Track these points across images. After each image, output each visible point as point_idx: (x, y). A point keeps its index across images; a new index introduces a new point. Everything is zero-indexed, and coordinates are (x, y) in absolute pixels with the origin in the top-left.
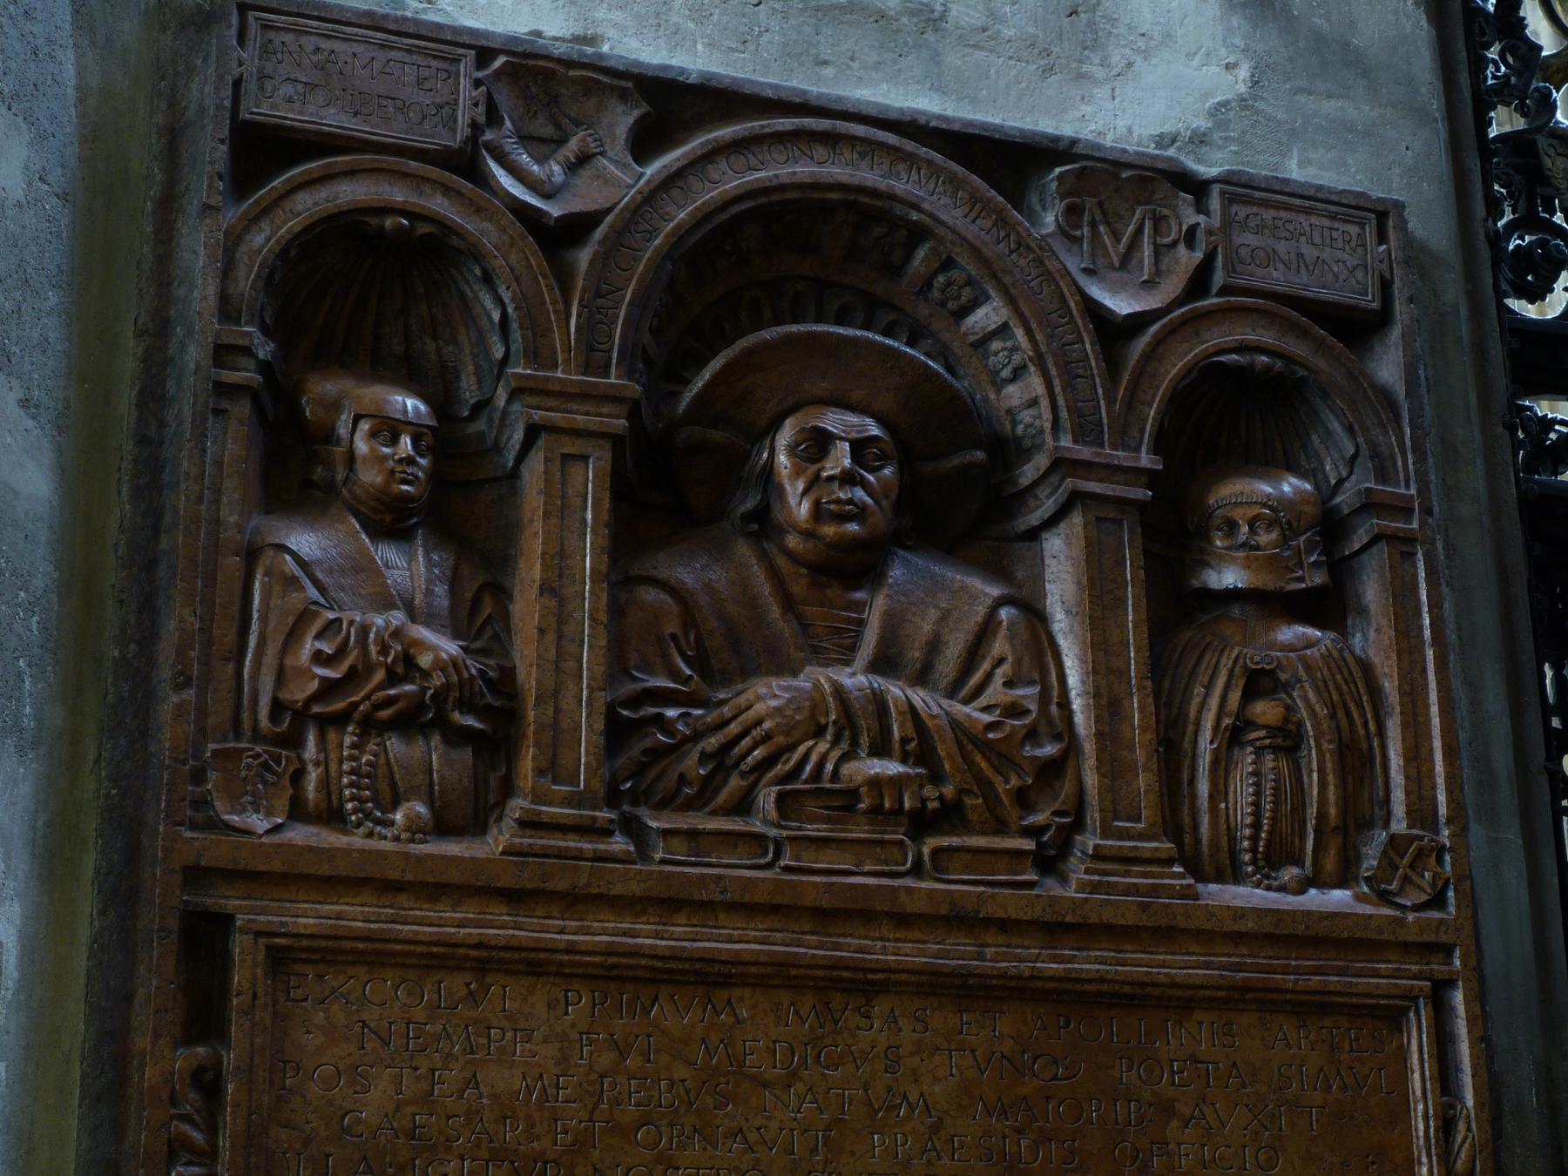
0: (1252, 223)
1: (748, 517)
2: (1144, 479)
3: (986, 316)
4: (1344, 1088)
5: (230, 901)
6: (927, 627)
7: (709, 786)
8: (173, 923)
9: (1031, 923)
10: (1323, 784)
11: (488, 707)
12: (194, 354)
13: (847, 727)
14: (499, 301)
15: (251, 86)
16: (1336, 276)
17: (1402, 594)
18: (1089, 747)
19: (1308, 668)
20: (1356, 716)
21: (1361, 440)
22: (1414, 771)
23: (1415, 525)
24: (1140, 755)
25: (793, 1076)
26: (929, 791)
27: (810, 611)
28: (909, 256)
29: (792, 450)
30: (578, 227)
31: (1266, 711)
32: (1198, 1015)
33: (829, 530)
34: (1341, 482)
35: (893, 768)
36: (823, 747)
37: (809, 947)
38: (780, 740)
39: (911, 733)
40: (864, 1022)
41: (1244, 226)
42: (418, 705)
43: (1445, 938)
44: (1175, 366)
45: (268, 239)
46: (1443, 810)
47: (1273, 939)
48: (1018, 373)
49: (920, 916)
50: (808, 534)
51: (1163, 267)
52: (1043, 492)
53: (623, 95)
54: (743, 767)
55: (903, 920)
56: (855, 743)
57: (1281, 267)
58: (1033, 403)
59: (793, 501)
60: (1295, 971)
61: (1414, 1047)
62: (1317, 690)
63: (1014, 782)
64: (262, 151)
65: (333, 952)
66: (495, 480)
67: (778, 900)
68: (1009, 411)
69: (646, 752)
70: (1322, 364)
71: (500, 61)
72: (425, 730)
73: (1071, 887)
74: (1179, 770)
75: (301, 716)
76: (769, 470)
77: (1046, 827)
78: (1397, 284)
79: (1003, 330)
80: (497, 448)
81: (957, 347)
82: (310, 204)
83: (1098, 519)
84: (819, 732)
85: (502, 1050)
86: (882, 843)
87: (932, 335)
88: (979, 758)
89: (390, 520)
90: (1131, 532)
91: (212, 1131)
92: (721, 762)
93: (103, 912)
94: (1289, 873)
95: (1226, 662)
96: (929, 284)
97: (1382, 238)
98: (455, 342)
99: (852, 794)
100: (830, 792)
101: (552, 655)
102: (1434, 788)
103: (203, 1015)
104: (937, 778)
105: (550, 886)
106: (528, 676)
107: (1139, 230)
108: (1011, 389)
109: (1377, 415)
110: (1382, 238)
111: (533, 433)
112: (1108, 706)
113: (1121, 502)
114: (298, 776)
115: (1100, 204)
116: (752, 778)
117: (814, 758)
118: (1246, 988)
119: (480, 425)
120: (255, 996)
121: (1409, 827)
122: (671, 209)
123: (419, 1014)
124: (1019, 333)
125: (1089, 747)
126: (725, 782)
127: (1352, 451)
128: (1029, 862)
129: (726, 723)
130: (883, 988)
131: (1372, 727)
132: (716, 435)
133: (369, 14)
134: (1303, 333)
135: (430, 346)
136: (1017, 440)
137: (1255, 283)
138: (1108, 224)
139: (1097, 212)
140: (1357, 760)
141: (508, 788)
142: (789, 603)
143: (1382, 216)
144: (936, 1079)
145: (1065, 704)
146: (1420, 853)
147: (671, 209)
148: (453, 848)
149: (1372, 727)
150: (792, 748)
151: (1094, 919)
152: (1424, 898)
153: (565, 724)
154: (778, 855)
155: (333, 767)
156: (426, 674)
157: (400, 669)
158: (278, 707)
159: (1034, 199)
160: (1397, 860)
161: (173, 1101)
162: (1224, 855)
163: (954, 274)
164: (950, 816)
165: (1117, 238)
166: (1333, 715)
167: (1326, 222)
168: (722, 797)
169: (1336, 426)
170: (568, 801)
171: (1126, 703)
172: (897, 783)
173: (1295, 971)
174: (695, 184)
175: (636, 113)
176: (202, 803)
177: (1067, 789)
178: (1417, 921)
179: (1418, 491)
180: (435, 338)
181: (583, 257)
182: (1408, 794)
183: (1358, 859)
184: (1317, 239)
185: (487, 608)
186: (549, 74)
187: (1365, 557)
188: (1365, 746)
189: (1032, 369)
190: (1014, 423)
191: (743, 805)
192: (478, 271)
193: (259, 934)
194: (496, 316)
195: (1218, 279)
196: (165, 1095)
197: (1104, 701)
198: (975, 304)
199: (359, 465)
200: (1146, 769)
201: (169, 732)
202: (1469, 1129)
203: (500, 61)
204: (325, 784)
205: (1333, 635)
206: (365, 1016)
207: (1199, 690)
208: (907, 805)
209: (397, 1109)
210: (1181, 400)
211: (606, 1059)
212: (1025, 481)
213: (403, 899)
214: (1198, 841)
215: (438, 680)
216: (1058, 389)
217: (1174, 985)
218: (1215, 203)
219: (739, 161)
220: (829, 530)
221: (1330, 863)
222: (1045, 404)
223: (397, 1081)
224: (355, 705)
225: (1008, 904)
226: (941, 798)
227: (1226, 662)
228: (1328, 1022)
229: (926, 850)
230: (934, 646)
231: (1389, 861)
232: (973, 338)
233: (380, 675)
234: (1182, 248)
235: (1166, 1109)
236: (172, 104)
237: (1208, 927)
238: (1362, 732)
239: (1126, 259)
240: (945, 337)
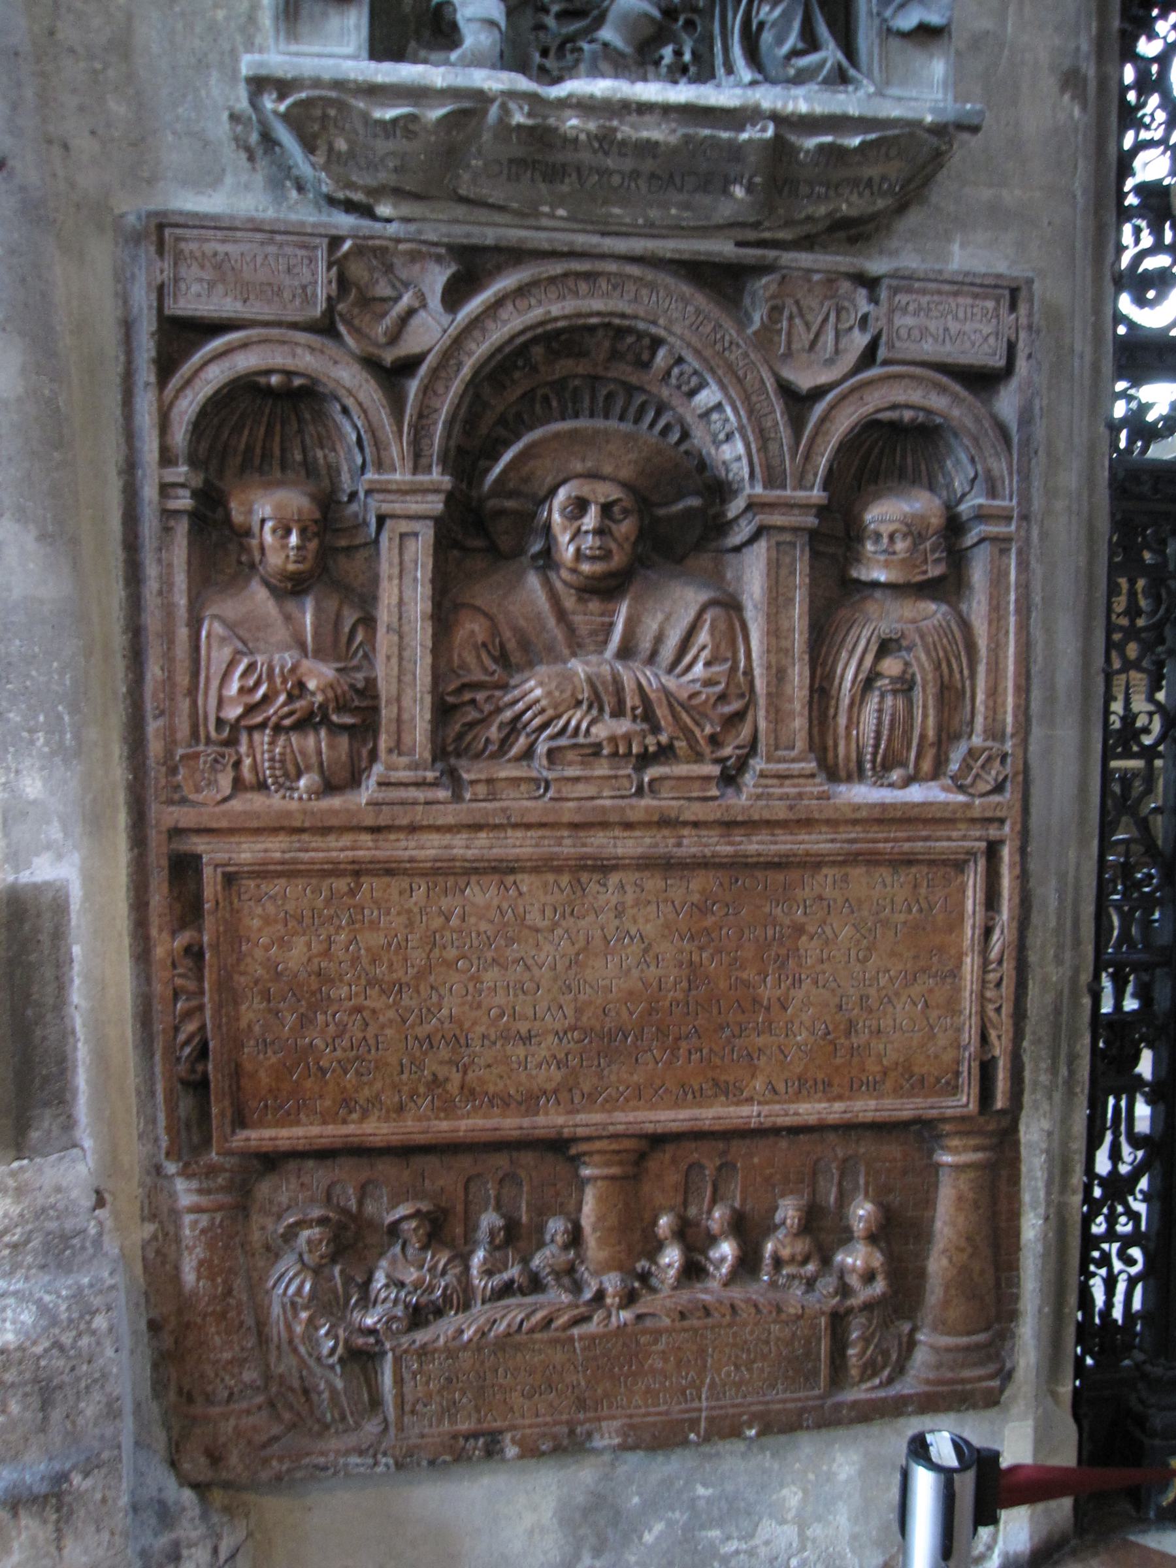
0: (911, 308)
1: (535, 557)
2: (814, 511)
3: (708, 396)
4: (921, 910)
5: (199, 845)
6: (655, 626)
7: (505, 743)
8: (165, 863)
9: (714, 822)
10: (925, 716)
11: (357, 708)
12: (149, 492)
13: (596, 701)
14: (355, 427)
15: (169, 289)
16: (973, 345)
17: (998, 579)
18: (762, 701)
19: (922, 637)
20: (955, 666)
21: (979, 467)
22: (993, 697)
23: (1013, 527)
24: (797, 706)
25: (555, 925)
26: (650, 740)
27: (578, 619)
28: (653, 354)
29: (562, 512)
30: (408, 366)
31: (891, 666)
32: (825, 871)
33: (586, 567)
34: (964, 495)
35: (624, 726)
36: (579, 714)
37: (568, 847)
38: (550, 712)
39: (637, 702)
40: (602, 890)
41: (904, 311)
42: (311, 714)
43: (999, 814)
44: (844, 423)
45: (191, 403)
46: (1009, 729)
47: (880, 821)
48: (729, 437)
49: (639, 823)
50: (574, 571)
51: (841, 346)
52: (743, 522)
53: (439, 259)
54: (528, 729)
55: (628, 826)
56: (601, 710)
57: (930, 340)
58: (739, 459)
59: (563, 548)
60: (895, 840)
61: (971, 883)
62: (928, 653)
63: (708, 730)
64: (181, 335)
65: (262, 872)
66: (365, 545)
67: (544, 820)
68: (724, 463)
69: (464, 725)
70: (956, 412)
71: (347, 245)
72: (316, 728)
73: (743, 800)
74: (827, 708)
75: (235, 726)
76: (548, 527)
77: (729, 758)
78: (1021, 345)
79: (719, 407)
80: (366, 524)
81: (689, 419)
82: (215, 376)
83: (778, 544)
84: (579, 703)
85: (371, 922)
86: (616, 777)
87: (673, 409)
88: (684, 715)
89: (291, 587)
90: (802, 551)
91: (200, 979)
92: (514, 727)
93: (131, 849)
94: (896, 775)
95: (866, 633)
96: (668, 373)
97: (1013, 307)
98: (334, 450)
99: (599, 746)
100: (582, 746)
101: (395, 672)
102: (1005, 712)
103: (189, 910)
104: (656, 729)
105: (397, 823)
106: (386, 688)
107: (828, 315)
108: (725, 447)
109: (994, 446)
110: (1013, 307)
111: (381, 520)
112: (779, 675)
113: (795, 530)
114: (237, 764)
115: (797, 302)
116: (533, 737)
117: (573, 723)
118: (858, 854)
119: (354, 507)
120: (217, 903)
121: (985, 740)
122: (473, 346)
123: (320, 902)
124: (728, 410)
125: (762, 701)
126: (517, 739)
127: (972, 475)
128: (714, 783)
129: (515, 702)
130: (615, 868)
131: (966, 672)
132: (510, 504)
133: (251, 220)
134: (943, 390)
135: (320, 454)
136: (730, 484)
137: (909, 357)
138: (802, 316)
139: (795, 309)
140: (950, 696)
141: (373, 756)
142: (561, 615)
143: (1014, 292)
144: (647, 921)
145: (749, 672)
146: (989, 759)
147: (473, 346)
148: (336, 802)
149: (966, 672)
150: (559, 716)
151: (756, 817)
152: (989, 788)
153: (406, 716)
154: (547, 789)
155: (259, 757)
156: (313, 694)
157: (296, 692)
158: (220, 722)
159: (747, 301)
160: (971, 762)
161: (174, 966)
162: (853, 765)
163: (685, 367)
164: (665, 753)
165: (808, 326)
166: (938, 667)
167: (969, 301)
168: (514, 751)
169: (963, 457)
170: (409, 767)
171: (790, 671)
172: (628, 738)
173: (895, 840)
174: (490, 325)
175: (449, 272)
176: (177, 788)
177: (745, 732)
178: (981, 804)
179: (1019, 503)
180: (322, 448)
181: (413, 386)
182: (986, 718)
183: (947, 760)
184: (961, 315)
185: (360, 637)
186: (384, 250)
187: (975, 550)
188: (959, 686)
189: (737, 435)
190: (727, 471)
191: (528, 754)
192: (338, 407)
193: (216, 866)
194: (354, 437)
195: (882, 353)
196: (169, 962)
197: (774, 671)
198: (702, 385)
199: (268, 552)
200: (802, 715)
201: (155, 747)
202: (1002, 932)
203: (347, 245)
204: (254, 766)
205: (944, 608)
206: (287, 907)
207: (844, 655)
208: (635, 750)
209: (309, 960)
210: (847, 447)
211: (438, 922)
212: (731, 515)
213: (305, 837)
214: (836, 756)
215: (319, 698)
216: (754, 450)
217: (808, 854)
218: (884, 294)
219: (521, 304)
220: (586, 567)
221: (927, 766)
222: (745, 461)
223: (309, 945)
224: (269, 718)
225: (695, 811)
226: (659, 744)
227: (866, 633)
228: (913, 870)
229: (646, 779)
230: (659, 639)
231: (966, 767)
232: (699, 412)
233: (282, 698)
234: (856, 331)
235: (799, 930)
236: (125, 302)
237: (834, 817)
238: (958, 676)
239: (813, 344)
240: (680, 410)
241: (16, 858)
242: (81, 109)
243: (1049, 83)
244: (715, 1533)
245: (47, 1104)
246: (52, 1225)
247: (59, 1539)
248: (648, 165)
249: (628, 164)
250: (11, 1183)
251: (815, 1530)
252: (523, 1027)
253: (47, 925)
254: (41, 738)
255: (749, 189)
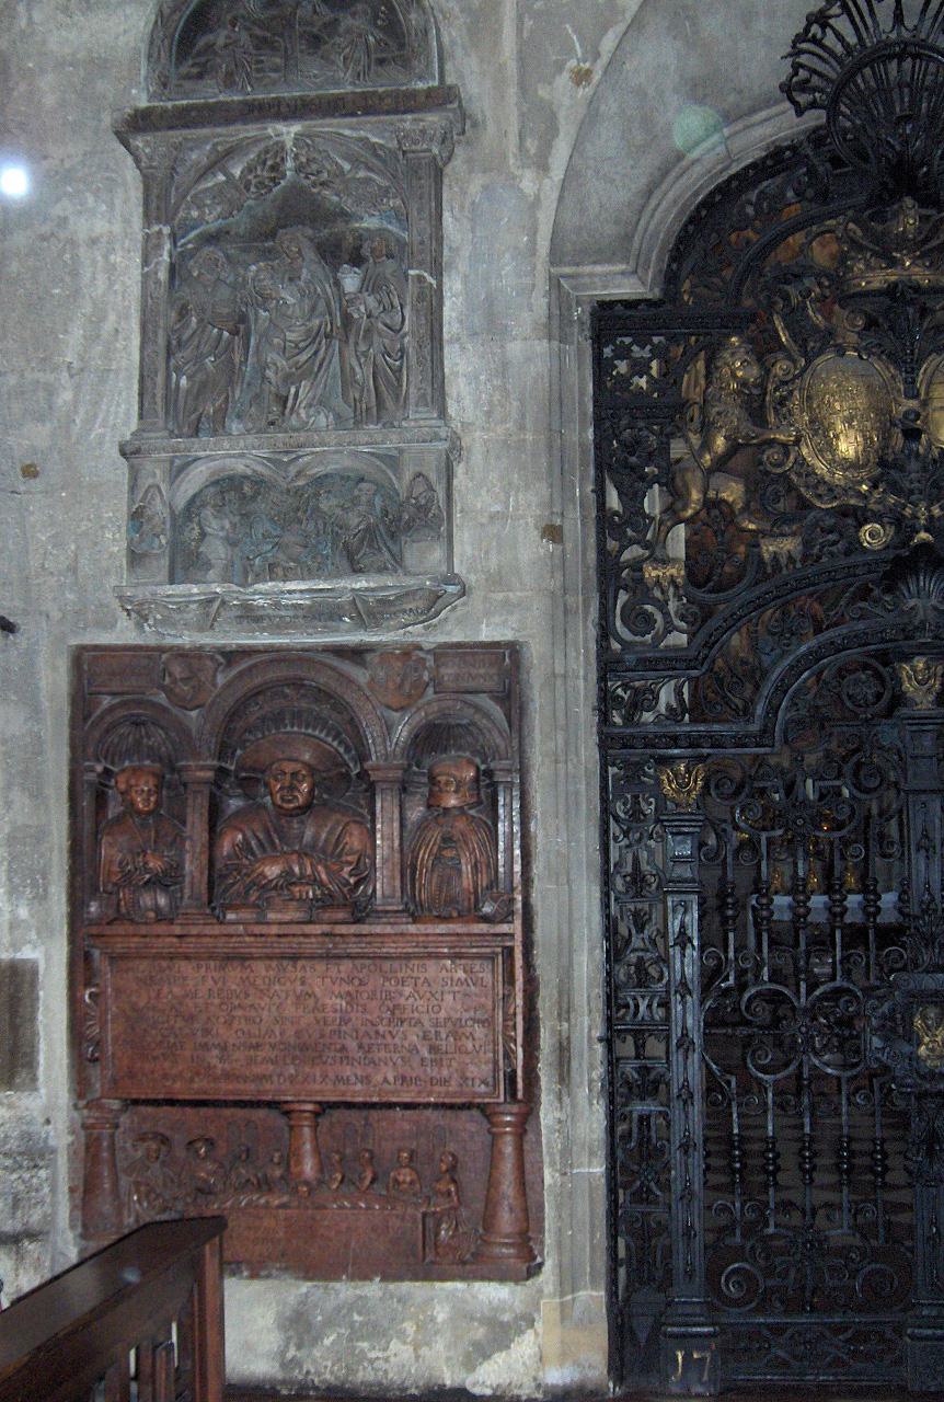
241: (15, 946)
242: (55, 599)
243: (535, 534)
244: (365, 1345)
245: (23, 1066)
246: (24, 1127)
247: (17, 1270)
248: (300, 613)
249: (291, 613)
250: (5, 1101)
251: (424, 1351)
252: (254, 1041)
253: (28, 978)
254: (28, 890)
255: (351, 618)
